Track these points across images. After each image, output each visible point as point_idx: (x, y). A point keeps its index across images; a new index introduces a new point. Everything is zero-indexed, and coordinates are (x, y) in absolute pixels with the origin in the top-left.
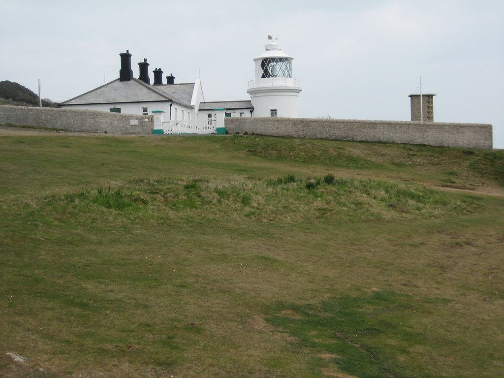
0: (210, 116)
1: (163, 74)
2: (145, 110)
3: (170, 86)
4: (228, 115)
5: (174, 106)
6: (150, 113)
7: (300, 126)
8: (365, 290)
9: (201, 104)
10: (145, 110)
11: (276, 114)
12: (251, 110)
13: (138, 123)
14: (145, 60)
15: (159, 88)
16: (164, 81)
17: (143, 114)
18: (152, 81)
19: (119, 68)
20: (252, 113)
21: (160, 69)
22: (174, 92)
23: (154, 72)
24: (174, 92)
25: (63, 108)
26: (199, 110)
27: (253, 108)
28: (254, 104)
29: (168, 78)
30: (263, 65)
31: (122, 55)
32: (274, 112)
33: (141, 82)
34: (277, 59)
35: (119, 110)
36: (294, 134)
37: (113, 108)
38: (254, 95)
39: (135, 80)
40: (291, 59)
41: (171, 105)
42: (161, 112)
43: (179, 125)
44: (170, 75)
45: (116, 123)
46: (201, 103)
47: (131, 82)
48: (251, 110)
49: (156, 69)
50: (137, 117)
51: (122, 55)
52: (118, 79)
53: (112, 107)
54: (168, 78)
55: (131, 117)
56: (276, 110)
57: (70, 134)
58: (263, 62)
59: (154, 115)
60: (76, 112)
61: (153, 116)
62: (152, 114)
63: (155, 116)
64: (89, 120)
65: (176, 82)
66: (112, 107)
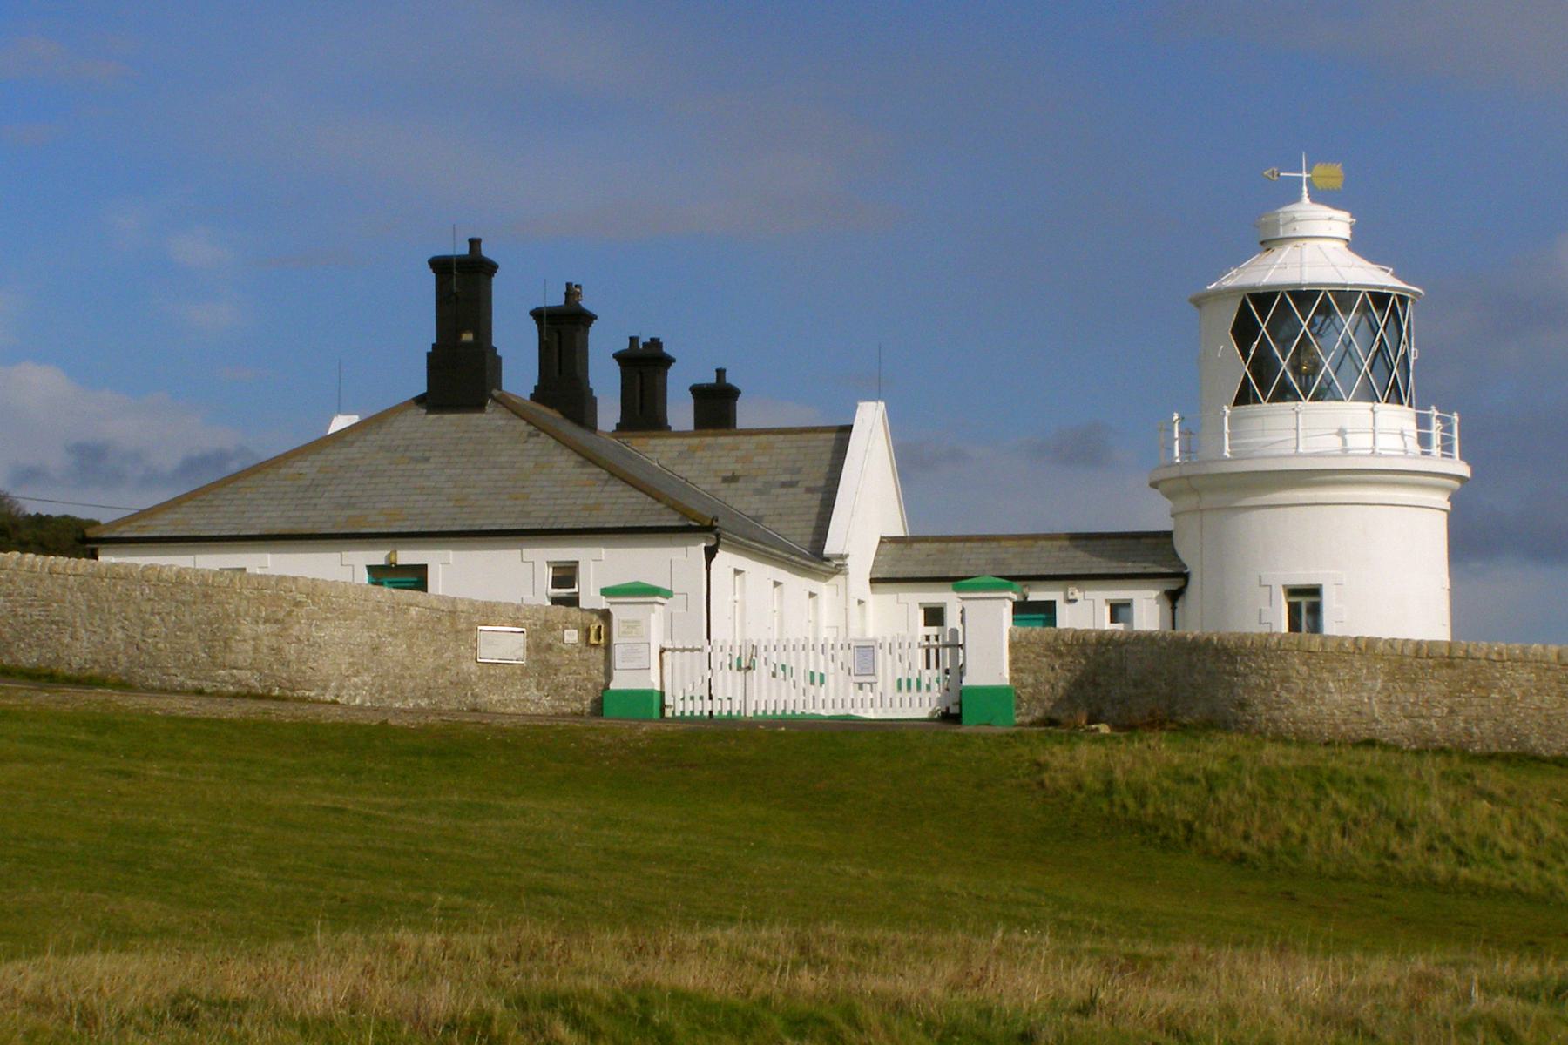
0: (934, 616)
1: (673, 373)
2: (565, 575)
3: (709, 440)
4: (1034, 612)
5: (724, 559)
6: (590, 593)
7: (1434, 688)
8: (1163, 1010)
9: (888, 546)
10: (565, 575)
11: (1315, 610)
12: (1173, 585)
13: (521, 653)
14: (571, 292)
15: (655, 452)
16: (680, 411)
17: (556, 601)
18: (609, 414)
19: (425, 335)
20: (1179, 604)
21: (655, 343)
22: (732, 479)
23: (621, 357)
24: (732, 479)
25: (107, 559)
26: (873, 581)
27: (1185, 577)
28: (1186, 550)
29: (699, 392)
30: (1244, 331)
31: (441, 266)
32: (1304, 601)
33: (551, 415)
34: (1283, 297)
35: (417, 577)
36: (1395, 726)
37: (382, 562)
38: (1189, 502)
39: (507, 403)
40: (569, 285)
41: (710, 554)
42: (654, 591)
43: (762, 672)
44: (711, 379)
45: (396, 650)
46: (883, 540)
47: (491, 419)
48: (1173, 585)
49: (633, 340)
50: (515, 614)
51: (441, 266)
52: (420, 400)
53: (378, 557)
54: (699, 392)
55: (490, 612)
56: (1315, 591)
57: (132, 702)
58: (1244, 311)
59: (613, 609)
60: (180, 579)
61: (606, 615)
62: (603, 603)
63: (621, 614)
64: (246, 628)
65: (747, 414)
66: (378, 557)
